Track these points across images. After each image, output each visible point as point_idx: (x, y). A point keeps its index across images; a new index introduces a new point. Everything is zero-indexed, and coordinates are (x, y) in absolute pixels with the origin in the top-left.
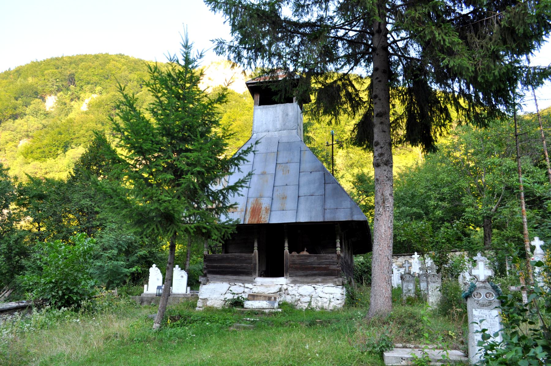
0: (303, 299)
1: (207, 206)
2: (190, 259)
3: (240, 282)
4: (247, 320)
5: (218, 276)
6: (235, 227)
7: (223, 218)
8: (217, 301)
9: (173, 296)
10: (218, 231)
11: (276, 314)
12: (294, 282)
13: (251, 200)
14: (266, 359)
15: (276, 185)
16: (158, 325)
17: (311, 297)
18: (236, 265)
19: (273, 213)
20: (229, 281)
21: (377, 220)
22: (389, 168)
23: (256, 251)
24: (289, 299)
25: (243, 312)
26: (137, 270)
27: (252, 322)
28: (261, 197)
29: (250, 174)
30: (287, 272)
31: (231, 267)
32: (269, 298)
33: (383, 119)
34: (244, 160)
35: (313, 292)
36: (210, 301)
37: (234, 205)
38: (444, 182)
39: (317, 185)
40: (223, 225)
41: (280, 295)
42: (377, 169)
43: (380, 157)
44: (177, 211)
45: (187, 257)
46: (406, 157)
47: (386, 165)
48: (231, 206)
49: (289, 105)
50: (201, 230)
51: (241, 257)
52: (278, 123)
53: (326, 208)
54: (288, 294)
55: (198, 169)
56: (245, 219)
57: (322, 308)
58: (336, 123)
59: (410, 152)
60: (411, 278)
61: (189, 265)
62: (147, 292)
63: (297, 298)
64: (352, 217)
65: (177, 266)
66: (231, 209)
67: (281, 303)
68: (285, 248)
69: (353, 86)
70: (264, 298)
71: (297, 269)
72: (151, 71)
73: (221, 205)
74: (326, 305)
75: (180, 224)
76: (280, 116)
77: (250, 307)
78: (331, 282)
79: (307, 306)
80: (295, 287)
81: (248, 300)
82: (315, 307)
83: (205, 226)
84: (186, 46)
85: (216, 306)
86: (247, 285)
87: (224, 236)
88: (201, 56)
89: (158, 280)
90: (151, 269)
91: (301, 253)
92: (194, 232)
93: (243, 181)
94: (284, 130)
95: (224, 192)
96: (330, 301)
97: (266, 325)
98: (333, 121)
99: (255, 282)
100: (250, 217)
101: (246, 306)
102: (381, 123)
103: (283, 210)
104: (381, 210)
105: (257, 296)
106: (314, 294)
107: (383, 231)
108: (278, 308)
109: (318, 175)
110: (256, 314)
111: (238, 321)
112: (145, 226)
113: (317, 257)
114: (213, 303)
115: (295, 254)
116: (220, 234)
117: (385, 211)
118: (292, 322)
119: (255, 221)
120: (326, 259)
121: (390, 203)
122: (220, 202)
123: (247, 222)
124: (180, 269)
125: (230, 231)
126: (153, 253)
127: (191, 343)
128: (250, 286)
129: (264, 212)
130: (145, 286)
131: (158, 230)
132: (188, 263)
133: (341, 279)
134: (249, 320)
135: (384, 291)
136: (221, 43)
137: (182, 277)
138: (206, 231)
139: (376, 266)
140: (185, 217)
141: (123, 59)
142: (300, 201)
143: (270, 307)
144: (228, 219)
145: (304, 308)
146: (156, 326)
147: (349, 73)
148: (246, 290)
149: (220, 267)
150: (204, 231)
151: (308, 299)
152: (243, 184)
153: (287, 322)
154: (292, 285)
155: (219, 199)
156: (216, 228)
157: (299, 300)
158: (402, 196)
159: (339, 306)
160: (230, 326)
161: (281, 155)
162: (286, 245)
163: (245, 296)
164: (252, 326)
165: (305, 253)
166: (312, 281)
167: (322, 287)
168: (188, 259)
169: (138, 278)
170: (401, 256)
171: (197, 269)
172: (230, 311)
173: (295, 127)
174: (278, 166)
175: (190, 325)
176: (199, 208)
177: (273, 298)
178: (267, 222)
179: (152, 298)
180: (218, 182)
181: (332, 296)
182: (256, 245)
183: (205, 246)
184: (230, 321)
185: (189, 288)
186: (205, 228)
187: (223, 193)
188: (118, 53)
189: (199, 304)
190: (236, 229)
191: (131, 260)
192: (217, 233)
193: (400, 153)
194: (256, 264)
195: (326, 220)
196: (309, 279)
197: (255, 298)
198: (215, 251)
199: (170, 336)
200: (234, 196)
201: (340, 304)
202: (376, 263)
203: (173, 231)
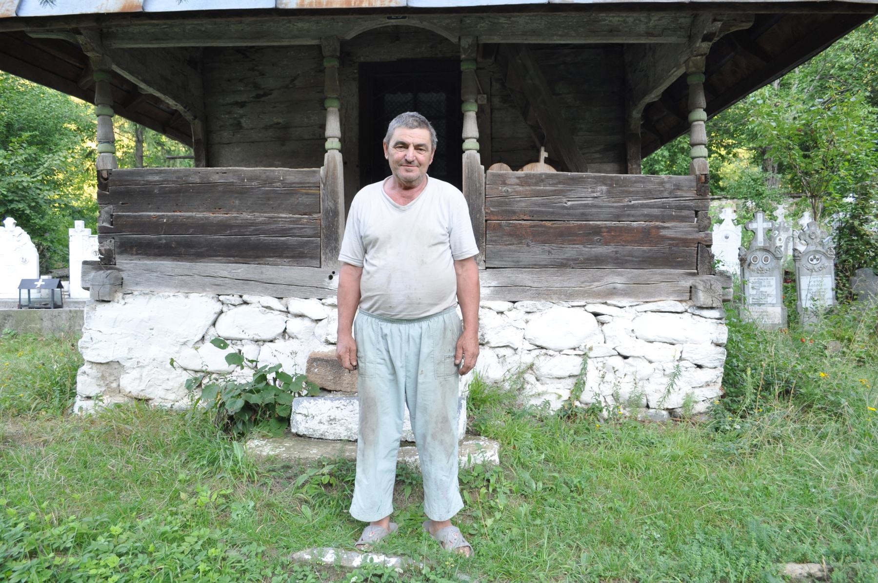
0: (546, 366)
3: (265, 292)
5: (167, 265)
18: (246, 216)
20: (219, 288)
31: (222, 227)
51: (269, 181)
60: (772, 263)
63: (528, 359)
74: (654, 392)
78: (669, 294)
79: (566, 395)
86: (296, 304)
89: (24, 261)
91: (529, 169)
101: (299, 424)
113: (610, 183)
145: (556, 405)
148: (295, 326)
149: (174, 226)
151: (573, 365)
154: (504, 305)
165: (541, 168)
182: (333, 127)
189: (86, 383)
196: (573, 279)
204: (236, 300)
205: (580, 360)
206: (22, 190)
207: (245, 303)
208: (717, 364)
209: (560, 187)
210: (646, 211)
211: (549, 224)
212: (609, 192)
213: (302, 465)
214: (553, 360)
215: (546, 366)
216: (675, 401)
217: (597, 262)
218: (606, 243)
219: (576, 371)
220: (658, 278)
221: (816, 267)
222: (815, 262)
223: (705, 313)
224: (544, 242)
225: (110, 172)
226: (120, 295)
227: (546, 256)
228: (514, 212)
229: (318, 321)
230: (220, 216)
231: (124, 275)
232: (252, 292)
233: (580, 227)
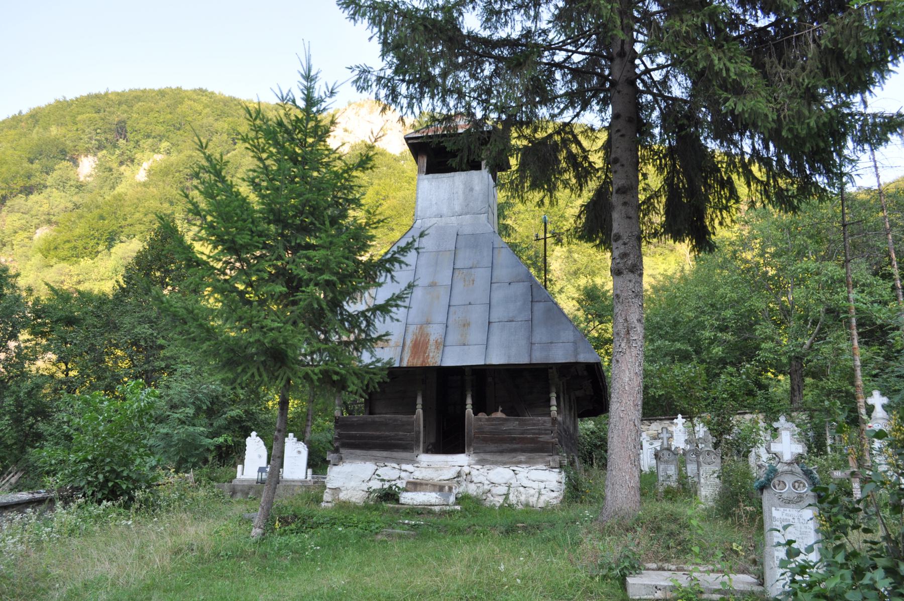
0: (495, 490)
1: (340, 337)
2: (313, 423)
4: (404, 524)
5: (358, 452)
6: (386, 372)
7: (366, 358)
8: (355, 492)
10: (358, 378)
11: (451, 513)
12: (482, 462)
14: (435, 588)
15: (452, 304)
16: (259, 531)
17: (509, 487)
19: (447, 349)
20: (376, 460)
21: (618, 361)
22: (637, 277)
23: (419, 411)
24: (472, 490)
25: (397, 511)
26: (226, 441)
27: (412, 526)
28: (428, 323)
29: (410, 286)
30: (470, 445)
31: (378, 437)
32: (441, 489)
33: (628, 198)
34: (400, 262)
35: (511, 479)
36: (345, 492)
37: (384, 336)
39: (519, 304)
40: (367, 369)
41: (458, 482)
43: (622, 259)
44: (292, 345)
47: (632, 272)
48: (380, 338)
49: (474, 173)
50: (330, 377)
54: (471, 482)
55: (326, 277)
57: (527, 505)
58: (551, 203)
59: (672, 251)
60: (672, 457)
61: (311, 434)
62: (242, 477)
63: (487, 487)
64: (576, 356)
66: (379, 342)
69: (579, 143)
70: (432, 488)
71: (485, 440)
73: (363, 336)
74: (533, 500)
75: (297, 366)
76: (461, 192)
78: (542, 463)
79: (501, 501)
80: (483, 471)
81: (407, 491)
82: (514, 502)
83: (337, 369)
85: (353, 500)
86: (404, 467)
87: (367, 386)
88: (332, 93)
89: (260, 457)
90: (248, 439)
91: (494, 415)
92: (319, 379)
93: (399, 297)
94: (466, 214)
95: (369, 314)
96: (540, 494)
97: (436, 531)
98: (547, 201)
99: (418, 462)
101: (402, 500)
102: (625, 204)
104: (623, 345)
105: (421, 484)
106: (513, 481)
108: (456, 504)
109: (521, 288)
110: (418, 514)
112: (239, 369)
114: (349, 495)
115: (482, 415)
117: (630, 347)
119: (418, 363)
120: (534, 425)
121: (638, 335)
122: (361, 331)
123: (405, 364)
124: (295, 439)
125: (378, 379)
126: (253, 414)
127: (312, 560)
128: (409, 467)
130: (240, 467)
131: (260, 376)
132: (308, 429)
133: (557, 458)
134: (408, 524)
135: (627, 477)
136: (364, 71)
137: (299, 452)
138: (339, 378)
139: (615, 437)
140: (305, 355)
141: (204, 98)
142: (491, 329)
143: (441, 502)
144: (374, 359)
146: (256, 532)
148: (403, 474)
149: (362, 437)
150: (335, 378)
151: (503, 490)
152: (399, 303)
153: (469, 527)
154: (479, 467)
155: (359, 327)
156: (355, 374)
157: (490, 491)
158: (657, 323)
159: (555, 502)
160: (377, 533)
161: (461, 254)
162: (469, 401)
163: (401, 484)
165: (499, 415)
166: (511, 460)
168: (310, 423)
169: (228, 454)
170: (656, 420)
171: (324, 440)
172: (377, 509)
173: (483, 210)
174: (457, 272)
175: (312, 531)
176: (327, 340)
177: (447, 488)
178: (438, 364)
179: (251, 487)
181: (542, 485)
182: (419, 401)
183: (337, 402)
184: (377, 525)
185: (310, 471)
186: (337, 373)
187: (366, 316)
188: (197, 87)
189: (327, 496)
190: (388, 374)
192: (356, 382)
193: (655, 253)
195: (534, 361)
196: (505, 458)
197: (418, 488)
198: (353, 411)
199: (280, 549)
201: (556, 498)
202: (615, 432)
203: (285, 378)
216: (541, 504)
217: (514, 451)
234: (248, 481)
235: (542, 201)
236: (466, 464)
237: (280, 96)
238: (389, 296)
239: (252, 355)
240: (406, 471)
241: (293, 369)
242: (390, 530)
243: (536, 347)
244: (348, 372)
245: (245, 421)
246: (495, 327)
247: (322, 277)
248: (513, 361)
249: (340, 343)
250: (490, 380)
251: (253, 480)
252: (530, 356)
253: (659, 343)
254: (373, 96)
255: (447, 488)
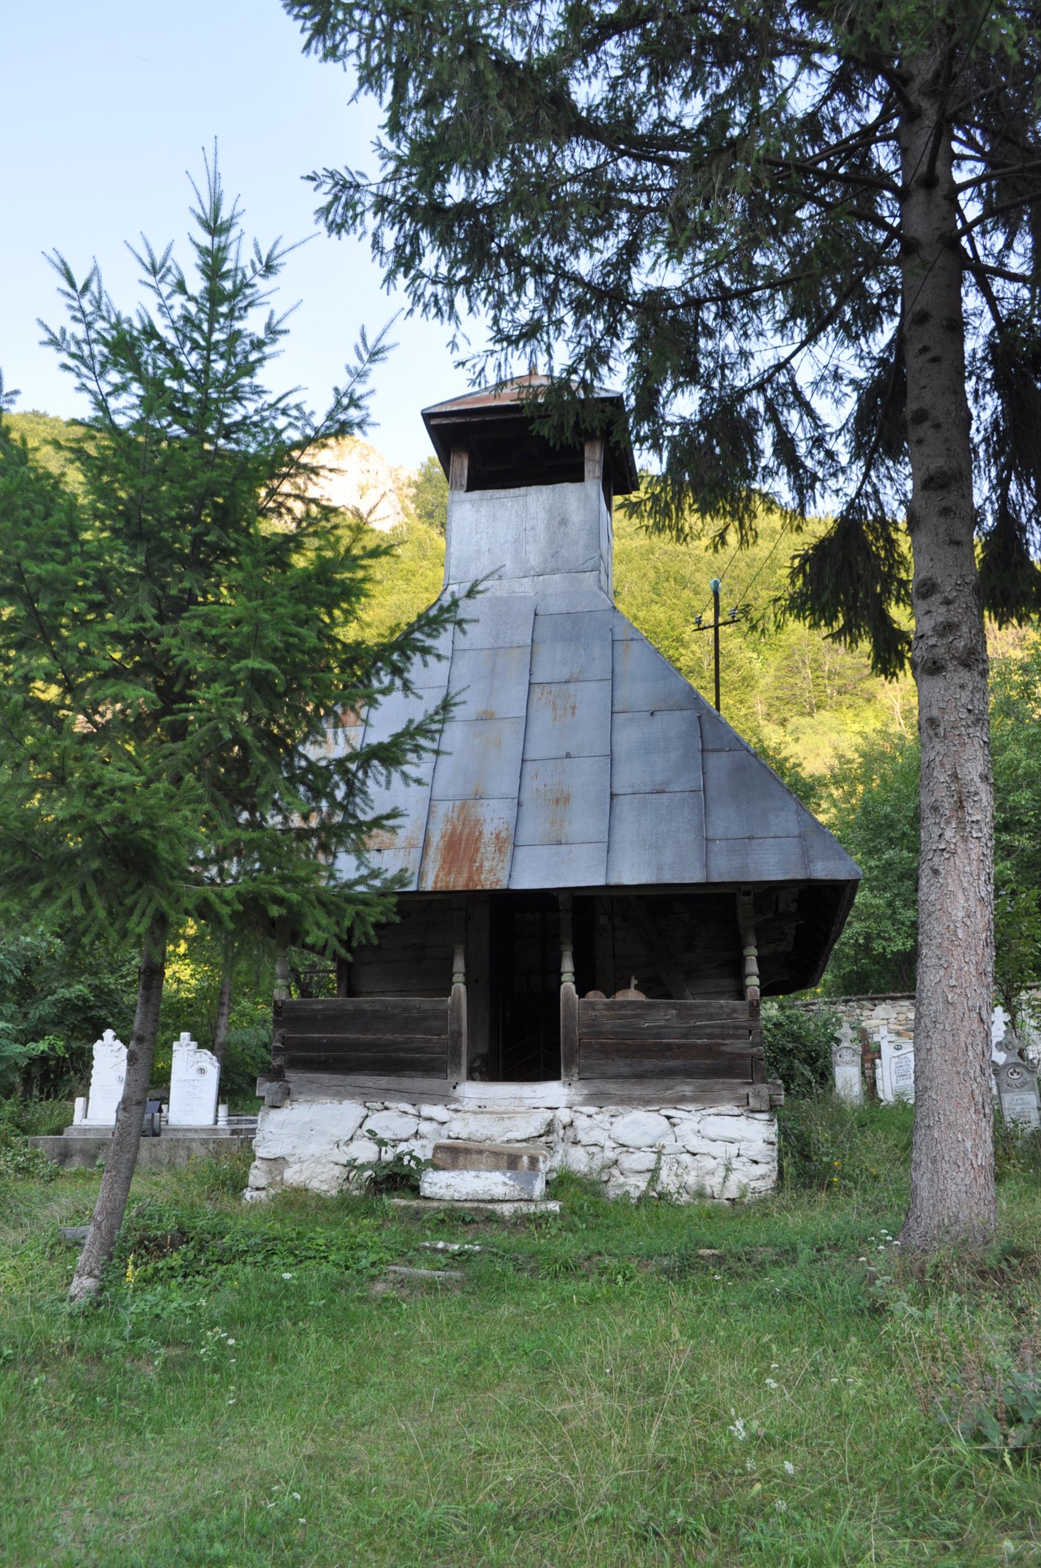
0: (629, 1161)
1: (286, 819)
2: (231, 1010)
3: (402, 1100)
4: (435, 1250)
5: (325, 1077)
6: (394, 900)
7: (346, 866)
8: (319, 1169)
9: (171, 1135)
10: (329, 913)
11: (540, 1220)
12: (598, 1099)
13: (442, 810)
14: (557, 1497)
15: (528, 756)
16: (89, 1283)
17: (659, 1153)
18: (389, 1037)
19: (521, 852)
20: (364, 1096)
21: (936, 872)
22: (978, 678)
23: (459, 987)
24: (579, 1161)
25: (416, 1215)
26: (52, 1048)
27: (454, 1256)
28: (478, 797)
29: (446, 705)
30: (570, 1063)
31: (370, 1046)
32: (512, 1162)
33: (952, 498)
34: (425, 651)
35: (664, 1135)
36: (296, 1167)
37: (388, 817)
38: (1020, 772)
39: (674, 755)
40: (345, 895)
41: (549, 1146)
42: (930, 682)
43: (941, 635)
44: (169, 831)
45: (222, 1004)
46: (857, 715)
47: (966, 665)
48: (377, 822)
49: (569, 489)
50: (264, 911)
52: (531, 548)
53: (711, 835)
54: (576, 1143)
55: (254, 663)
56: (421, 875)
57: (700, 1194)
58: (743, 541)
59: (869, 700)
61: (228, 1030)
62: (85, 1122)
63: (610, 1155)
64: (806, 867)
65: (185, 1035)
66: (375, 831)
67: (555, 1175)
68: (564, 978)
69: (807, 409)
70: (492, 1160)
71: (605, 1052)
72: (73, 285)
73: (338, 818)
74: (713, 1183)
75: (181, 883)
76: (541, 528)
77: (447, 1194)
78: (730, 1100)
79: (643, 1186)
80: (602, 1118)
81: (437, 1168)
82: (672, 1189)
83: (280, 891)
84: (215, 227)
85: (314, 1184)
86: (427, 1110)
87: (350, 931)
88: (269, 268)
90: (98, 1046)
91: (620, 997)
92: (234, 916)
93: (422, 730)
94: (553, 572)
95: (353, 767)
96: (728, 1169)
97: (511, 1271)
98: (732, 538)
99: (456, 1100)
100: (442, 868)
101: (426, 1189)
102: (945, 512)
103: (559, 843)
104: (949, 834)
105: (467, 1151)
106: (668, 1141)
107: (961, 914)
108: (549, 1197)
109: (676, 723)
110: (466, 1223)
111: (403, 1254)
112: (36, 890)
114: (306, 1174)
115: (593, 996)
116: (338, 923)
117: (965, 840)
118: (606, 1260)
119: (458, 882)
120: (710, 1017)
121: (983, 810)
122: (334, 804)
123: (429, 885)
125: (375, 914)
126: (110, 993)
127: (216, 1369)
128: (438, 1112)
129: (491, 849)
130: (79, 1102)
131: (89, 906)
132: (223, 1021)
133: (764, 1089)
134: (444, 1251)
135: (969, 1144)
136: (346, 186)
137: (202, 1071)
138: (283, 911)
139: (936, 1048)
140: (206, 863)
141: (41, 427)
142: (617, 810)
143: (516, 1195)
144: (364, 871)
145: (635, 1194)
146: (83, 1285)
147: (793, 361)
148: (425, 1127)
149: (332, 1045)
150: (275, 911)
151: (647, 1160)
152: (422, 741)
153: (589, 1258)
154: (592, 1110)
155: (331, 797)
156: (322, 903)
157: (616, 1162)
158: (886, 816)
159: (760, 1185)
160: (373, 1278)
161: (545, 653)
162: (568, 966)
163: (423, 1151)
164: (456, 1274)
165: (633, 995)
166: (661, 1094)
167: (696, 1117)
168: (225, 1010)
169: (60, 1074)
170: (884, 999)
171: (254, 1042)
172: (370, 1213)
173: (590, 564)
174: (537, 691)
175: (221, 1269)
176: (255, 825)
177: (525, 1160)
178: (502, 885)
179: (102, 1144)
180: (330, 732)
181: (733, 1150)
182: (459, 965)
183: (278, 969)
184: (373, 1257)
185: (223, 1109)
186: (279, 901)
187: (347, 771)
188: (30, 409)
189: (257, 1176)
190: (397, 905)
191: (34, 1013)
192: (324, 921)
193: (840, 704)
194: (460, 1034)
195: (715, 878)
196: (649, 1089)
197: (461, 1160)
198: (309, 985)
199: (137, 1334)
200: (388, 782)
201: (763, 1177)
202: (936, 1036)
203: (150, 911)
204: (378, 1106)
205: (654, 1156)
206: (106, 994)
207: (386, 1108)
208: (769, 1159)
209: (639, 1011)
210: (708, 1031)
211: (629, 1042)
212: (678, 1015)
213: (425, 1210)
214: (634, 1156)
215: (629, 1161)
216: (732, 1192)
218: (677, 1058)
219: (652, 1166)
220: (720, 1086)
221: (1017, 1083)
222: (1016, 1076)
223: (758, 1116)
224: (626, 1057)
225: (284, 1002)
226: (288, 1102)
227: (628, 1069)
228: (601, 1033)
229: (443, 1123)
230: (369, 1037)
231: (291, 1086)
232: (392, 1099)
233: (655, 1045)
234: (96, 1130)
235: (722, 536)
236: (562, 1103)
237: (147, 261)
238: (399, 728)
239: (71, 857)
240: (431, 1119)
241: (170, 891)
242: (404, 1270)
243: (716, 847)
244: (304, 897)
245: (91, 1008)
246: (625, 806)
247: (243, 663)
248: (669, 877)
249: (287, 831)
250: (603, 920)
251: (107, 1129)
252: (706, 865)
253: (889, 854)
254: (368, 239)
255: (525, 1160)
